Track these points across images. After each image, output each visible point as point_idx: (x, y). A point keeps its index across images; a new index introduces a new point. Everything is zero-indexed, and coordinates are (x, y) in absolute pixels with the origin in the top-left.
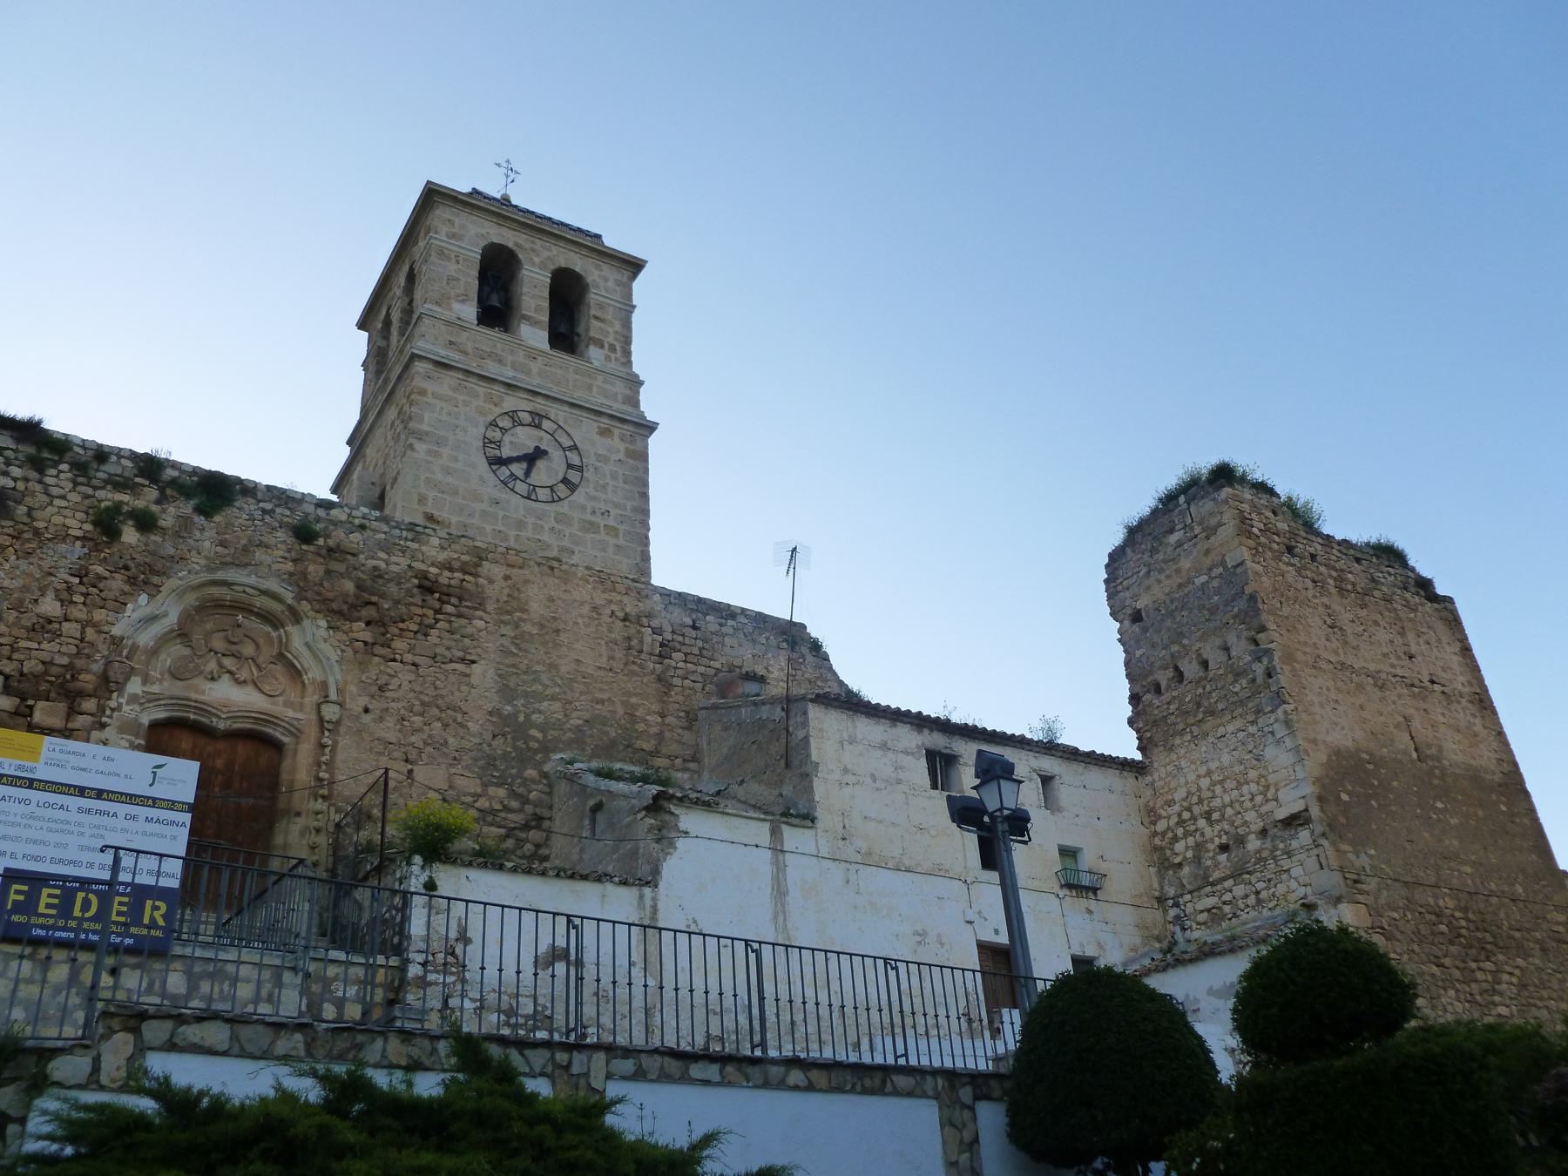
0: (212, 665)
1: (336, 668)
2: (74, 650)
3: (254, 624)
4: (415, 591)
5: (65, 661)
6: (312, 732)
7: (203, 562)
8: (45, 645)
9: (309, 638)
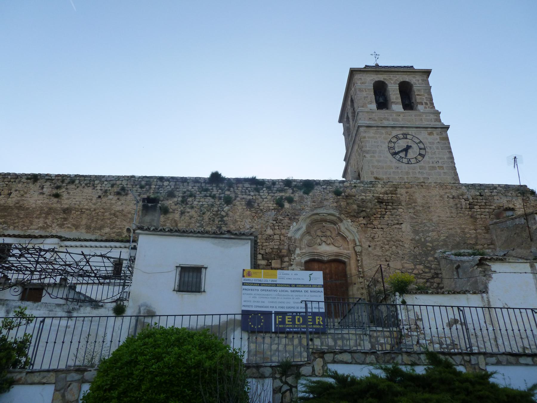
0: (319, 241)
1: (357, 235)
2: (279, 243)
3: (328, 225)
4: (377, 204)
5: (277, 247)
6: (353, 256)
7: (309, 209)
8: (271, 243)
9: (346, 226)
